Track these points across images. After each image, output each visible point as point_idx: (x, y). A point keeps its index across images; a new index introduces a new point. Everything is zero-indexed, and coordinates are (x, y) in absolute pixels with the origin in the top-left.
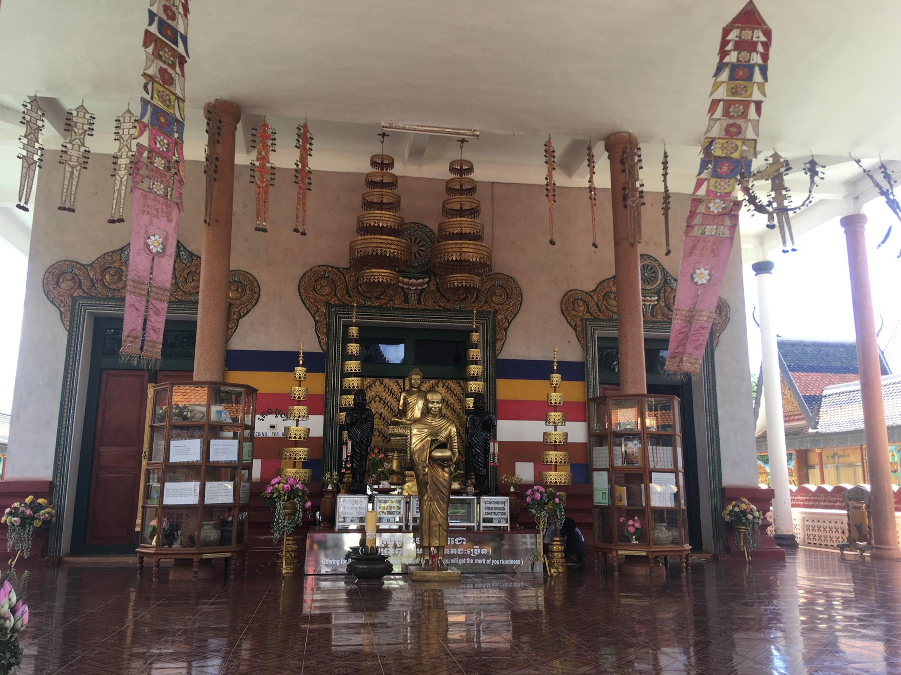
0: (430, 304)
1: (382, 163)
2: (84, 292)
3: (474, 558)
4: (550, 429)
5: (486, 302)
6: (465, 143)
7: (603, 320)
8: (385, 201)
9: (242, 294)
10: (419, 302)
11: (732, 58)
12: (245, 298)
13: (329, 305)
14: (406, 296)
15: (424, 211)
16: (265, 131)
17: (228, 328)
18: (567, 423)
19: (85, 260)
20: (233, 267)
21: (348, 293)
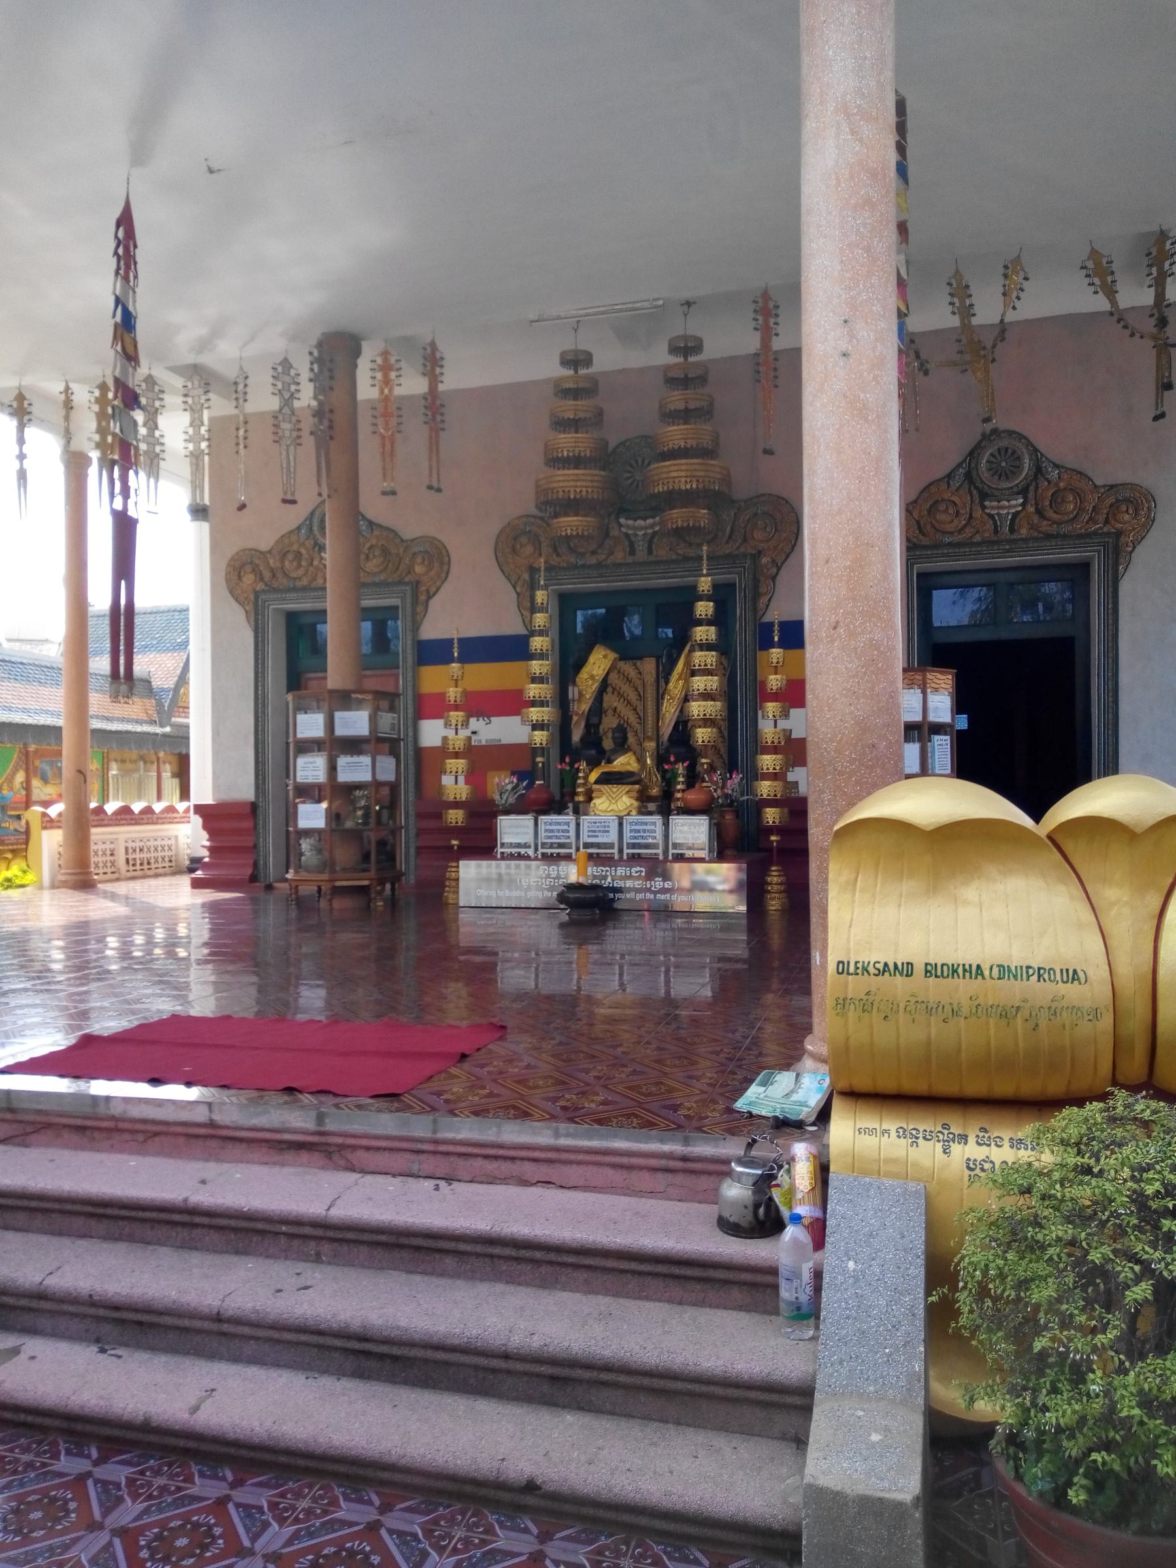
1: (576, 360)
2: (266, 585)
3: (655, 893)
4: (450, 733)
6: (693, 307)
7: (925, 547)
8: (692, 406)
12: (433, 572)
14: (632, 545)
19: (264, 546)
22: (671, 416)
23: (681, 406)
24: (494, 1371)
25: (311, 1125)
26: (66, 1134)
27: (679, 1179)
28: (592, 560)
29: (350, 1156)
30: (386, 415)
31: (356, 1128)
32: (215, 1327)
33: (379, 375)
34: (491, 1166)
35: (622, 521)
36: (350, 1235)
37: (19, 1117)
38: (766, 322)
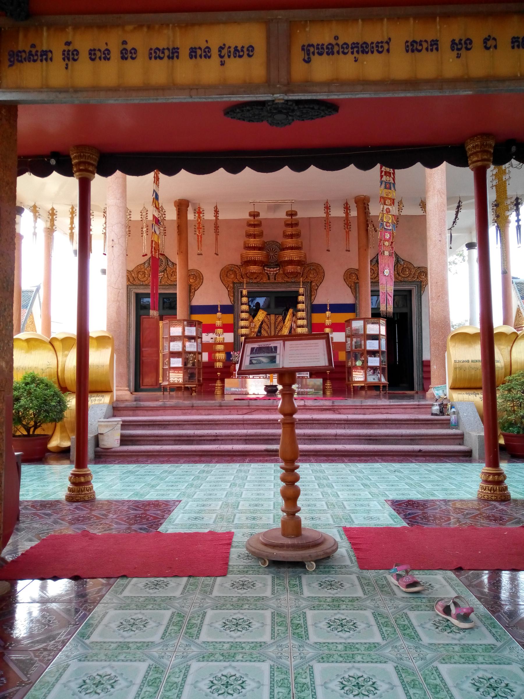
0: (280, 280)
5: (307, 277)
9: (194, 280)
10: (275, 279)
11: (384, 178)
13: (234, 283)
14: (269, 276)
15: (275, 234)
16: (199, 210)
17: (190, 296)
18: (224, 334)
20: (190, 268)
21: (242, 277)
22: (286, 236)
23: (290, 233)
24: (399, 440)
25: (331, 404)
26: (263, 411)
27: (417, 410)
28: (255, 281)
29: (339, 410)
30: (199, 228)
31: (342, 404)
32: (335, 437)
33: (197, 215)
34: (374, 411)
35: (265, 268)
36: (353, 422)
37: (250, 408)
38: (327, 211)
